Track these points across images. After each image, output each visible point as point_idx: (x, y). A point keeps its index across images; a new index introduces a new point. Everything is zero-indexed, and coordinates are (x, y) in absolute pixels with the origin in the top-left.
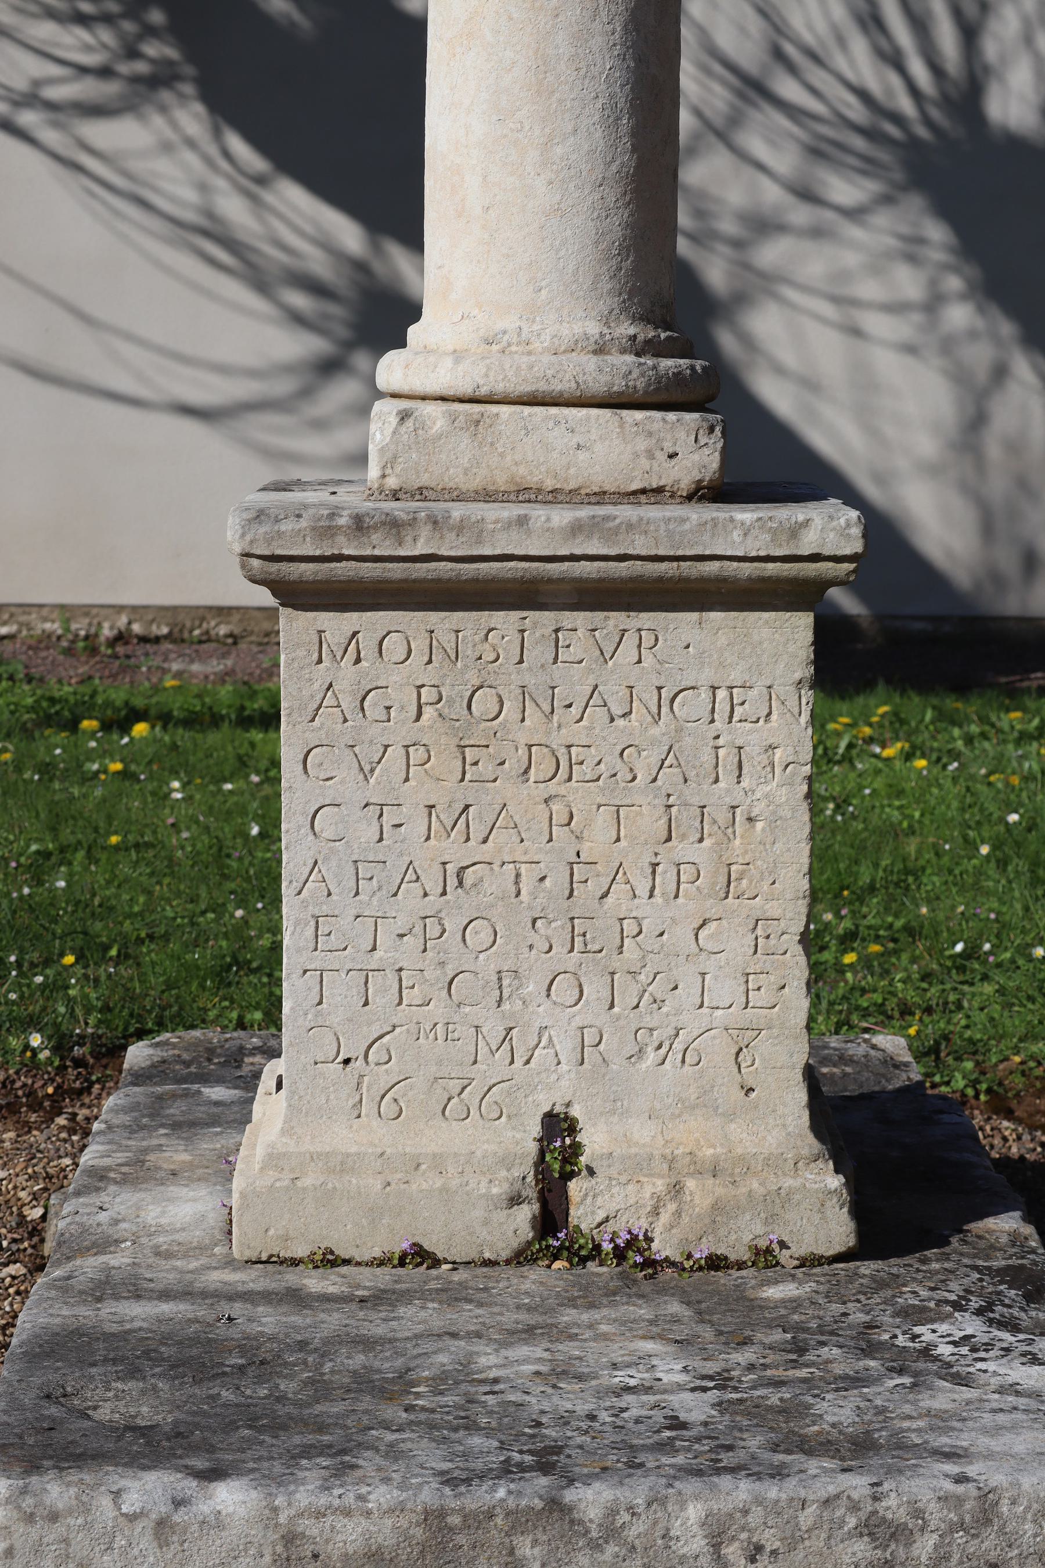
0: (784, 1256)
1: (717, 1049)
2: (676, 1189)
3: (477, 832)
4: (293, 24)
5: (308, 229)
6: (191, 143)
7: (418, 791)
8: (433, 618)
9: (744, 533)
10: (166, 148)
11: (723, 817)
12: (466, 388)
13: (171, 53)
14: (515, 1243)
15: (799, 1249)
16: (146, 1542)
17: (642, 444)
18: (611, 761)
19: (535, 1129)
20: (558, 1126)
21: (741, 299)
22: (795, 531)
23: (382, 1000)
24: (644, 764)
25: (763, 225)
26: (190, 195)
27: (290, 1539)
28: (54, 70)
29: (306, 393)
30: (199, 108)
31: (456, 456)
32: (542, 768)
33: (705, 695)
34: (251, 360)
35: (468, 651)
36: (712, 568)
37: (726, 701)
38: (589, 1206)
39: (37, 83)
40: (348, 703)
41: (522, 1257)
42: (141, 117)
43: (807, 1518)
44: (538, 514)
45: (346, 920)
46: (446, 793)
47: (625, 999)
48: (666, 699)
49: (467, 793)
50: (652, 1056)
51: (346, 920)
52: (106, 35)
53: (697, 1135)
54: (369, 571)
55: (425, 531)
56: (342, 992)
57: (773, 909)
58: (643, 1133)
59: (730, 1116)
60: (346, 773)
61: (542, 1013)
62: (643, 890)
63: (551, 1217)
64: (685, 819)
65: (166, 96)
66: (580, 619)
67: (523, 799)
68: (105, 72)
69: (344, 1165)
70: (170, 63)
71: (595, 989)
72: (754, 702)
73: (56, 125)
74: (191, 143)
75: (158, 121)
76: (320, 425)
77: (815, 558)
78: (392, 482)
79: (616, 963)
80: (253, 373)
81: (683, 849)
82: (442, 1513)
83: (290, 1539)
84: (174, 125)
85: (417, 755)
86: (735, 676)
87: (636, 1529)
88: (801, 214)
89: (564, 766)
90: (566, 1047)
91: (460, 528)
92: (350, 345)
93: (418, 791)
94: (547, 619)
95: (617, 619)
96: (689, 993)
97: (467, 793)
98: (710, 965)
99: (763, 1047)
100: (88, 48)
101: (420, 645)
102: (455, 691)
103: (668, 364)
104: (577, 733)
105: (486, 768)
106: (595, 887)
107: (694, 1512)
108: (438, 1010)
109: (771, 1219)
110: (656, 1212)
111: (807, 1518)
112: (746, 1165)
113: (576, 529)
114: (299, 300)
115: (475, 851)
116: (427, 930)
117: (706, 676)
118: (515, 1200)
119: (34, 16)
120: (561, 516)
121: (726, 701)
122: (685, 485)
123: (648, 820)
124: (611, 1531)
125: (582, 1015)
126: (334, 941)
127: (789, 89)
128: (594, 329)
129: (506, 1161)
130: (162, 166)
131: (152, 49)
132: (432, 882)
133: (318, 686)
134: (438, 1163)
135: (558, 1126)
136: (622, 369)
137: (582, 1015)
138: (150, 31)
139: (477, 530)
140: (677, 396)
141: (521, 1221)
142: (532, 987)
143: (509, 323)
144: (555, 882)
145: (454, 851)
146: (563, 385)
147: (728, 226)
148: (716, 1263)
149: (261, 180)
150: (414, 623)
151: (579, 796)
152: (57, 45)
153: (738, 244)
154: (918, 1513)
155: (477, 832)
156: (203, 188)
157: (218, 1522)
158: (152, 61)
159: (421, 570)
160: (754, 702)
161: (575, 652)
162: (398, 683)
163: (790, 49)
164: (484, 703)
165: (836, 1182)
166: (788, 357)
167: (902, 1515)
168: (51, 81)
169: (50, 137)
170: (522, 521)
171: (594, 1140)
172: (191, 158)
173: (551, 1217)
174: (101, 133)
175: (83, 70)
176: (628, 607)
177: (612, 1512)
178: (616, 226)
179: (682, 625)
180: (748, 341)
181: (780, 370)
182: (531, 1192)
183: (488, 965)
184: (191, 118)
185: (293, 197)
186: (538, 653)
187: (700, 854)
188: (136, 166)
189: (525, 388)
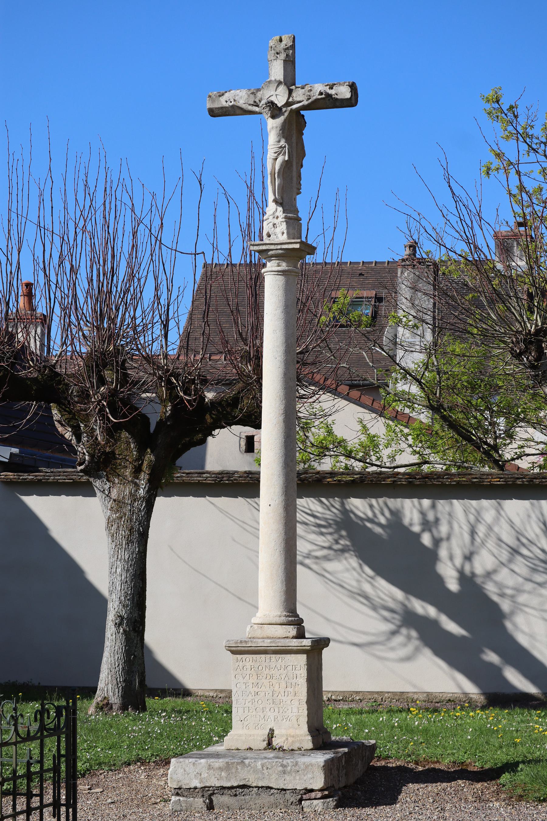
0: (303, 749)
1: (294, 719)
2: (287, 739)
3: (259, 687)
4: (381, 534)
5: (387, 593)
6: (354, 569)
7: (251, 681)
8: (253, 655)
9: (296, 643)
10: (347, 570)
11: (294, 684)
12: (260, 623)
13: (348, 543)
14: (264, 747)
15: (305, 748)
16: (192, 766)
17: (285, 630)
18: (278, 676)
19: (268, 731)
20: (272, 731)
21: (512, 613)
22: (301, 643)
23: (246, 711)
24: (283, 677)
25: (518, 590)
26: (354, 583)
27: (209, 765)
28: (315, 547)
29: (388, 639)
30: (355, 558)
31: (259, 633)
32: (269, 677)
33: (291, 666)
34: (373, 631)
35: (258, 660)
36: (290, 648)
37: (294, 668)
38: (276, 742)
39: (310, 551)
40: (241, 668)
41: (265, 749)
42: (340, 561)
43: (274, 764)
44: (266, 640)
45: (241, 700)
46: (255, 681)
47: (281, 711)
48: (286, 667)
49: (258, 681)
50: (285, 720)
51: (241, 700)
52: (329, 537)
53: (292, 732)
54: (243, 648)
55: (250, 643)
56: (241, 711)
57: (302, 698)
58: (284, 732)
59: (296, 729)
60: (241, 678)
61: (269, 713)
62: (283, 695)
63: (270, 743)
64: (289, 685)
65: (347, 555)
66: (274, 656)
67: (266, 682)
68: (330, 548)
69: (240, 736)
70: (348, 546)
71: (277, 710)
72: (298, 668)
73: (316, 563)
74: (354, 569)
75: (344, 562)
76: (393, 649)
77: (304, 646)
78: (249, 636)
79: (279, 706)
80: (373, 634)
81: (289, 689)
82: (228, 762)
83: (209, 765)
84: (350, 564)
85: (251, 675)
86: (296, 664)
87: (252, 765)
88: (529, 586)
89: (272, 677)
90: (273, 719)
91: (255, 642)
92: (400, 627)
93: (251, 681)
94: (268, 656)
95: (279, 656)
96: (290, 711)
97: (258, 681)
98: (293, 706)
99: (301, 719)
100: (324, 541)
101: (251, 659)
102: (256, 666)
103: (290, 619)
104: (273, 672)
105: (261, 677)
106: (276, 695)
107: (260, 763)
108: (254, 713)
109: (301, 743)
110: (284, 742)
111: (274, 764)
112: (298, 736)
113: (271, 642)
114: (386, 614)
115: (259, 690)
116: (253, 701)
117: (291, 664)
118: (264, 741)
119: (309, 533)
120: (269, 641)
121: (294, 668)
122: (291, 636)
123: (283, 685)
124: (249, 765)
125: (275, 714)
126: (240, 703)
127: (525, 552)
128: (279, 613)
129: (263, 735)
130: (347, 575)
131: (342, 542)
132: (253, 694)
133: (237, 665)
134: (254, 735)
135: (272, 731)
136: (283, 619)
137: (275, 714)
138: (341, 537)
139: (257, 642)
140: (292, 623)
141: (265, 744)
142: (268, 710)
143: (267, 613)
144: (271, 694)
145: (256, 690)
146: (273, 622)
147: (509, 592)
148: (292, 750)
149: (372, 578)
150: (250, 656)
151: (274, 681)
152: (316, 541)
153: (512, 596)
154: (288, 764)
155: (259, 687)
156: (358, 581)
157: (201, 763)
158: (342, 545)
159: (250, 648)
160: (298, 668)
161: (273, 660)
162: (248, 665)
163: (524, 541)
164: (260, 668)
165: (310, 738)
166: (526, 630)
167: (286, 764)
168: (314, 550)
169: (314, 567)
170: (263, 641)
171: (276, 733)
172: (355, 574)
173: (270, 743)
174: (330, 566)
175: (324, 548)
176: (280, 654)
177: (249, 763)
178: (283, 598)
179: (288, 656)
180: (515, 625)
181: (523, 632)
182: (267, 739)
183: (261, 706)
184: (354, 562)
185: (382, 583)
186: (268, 660)
187: (291, 690)
188: (340, 576)
189: (268, 622)
